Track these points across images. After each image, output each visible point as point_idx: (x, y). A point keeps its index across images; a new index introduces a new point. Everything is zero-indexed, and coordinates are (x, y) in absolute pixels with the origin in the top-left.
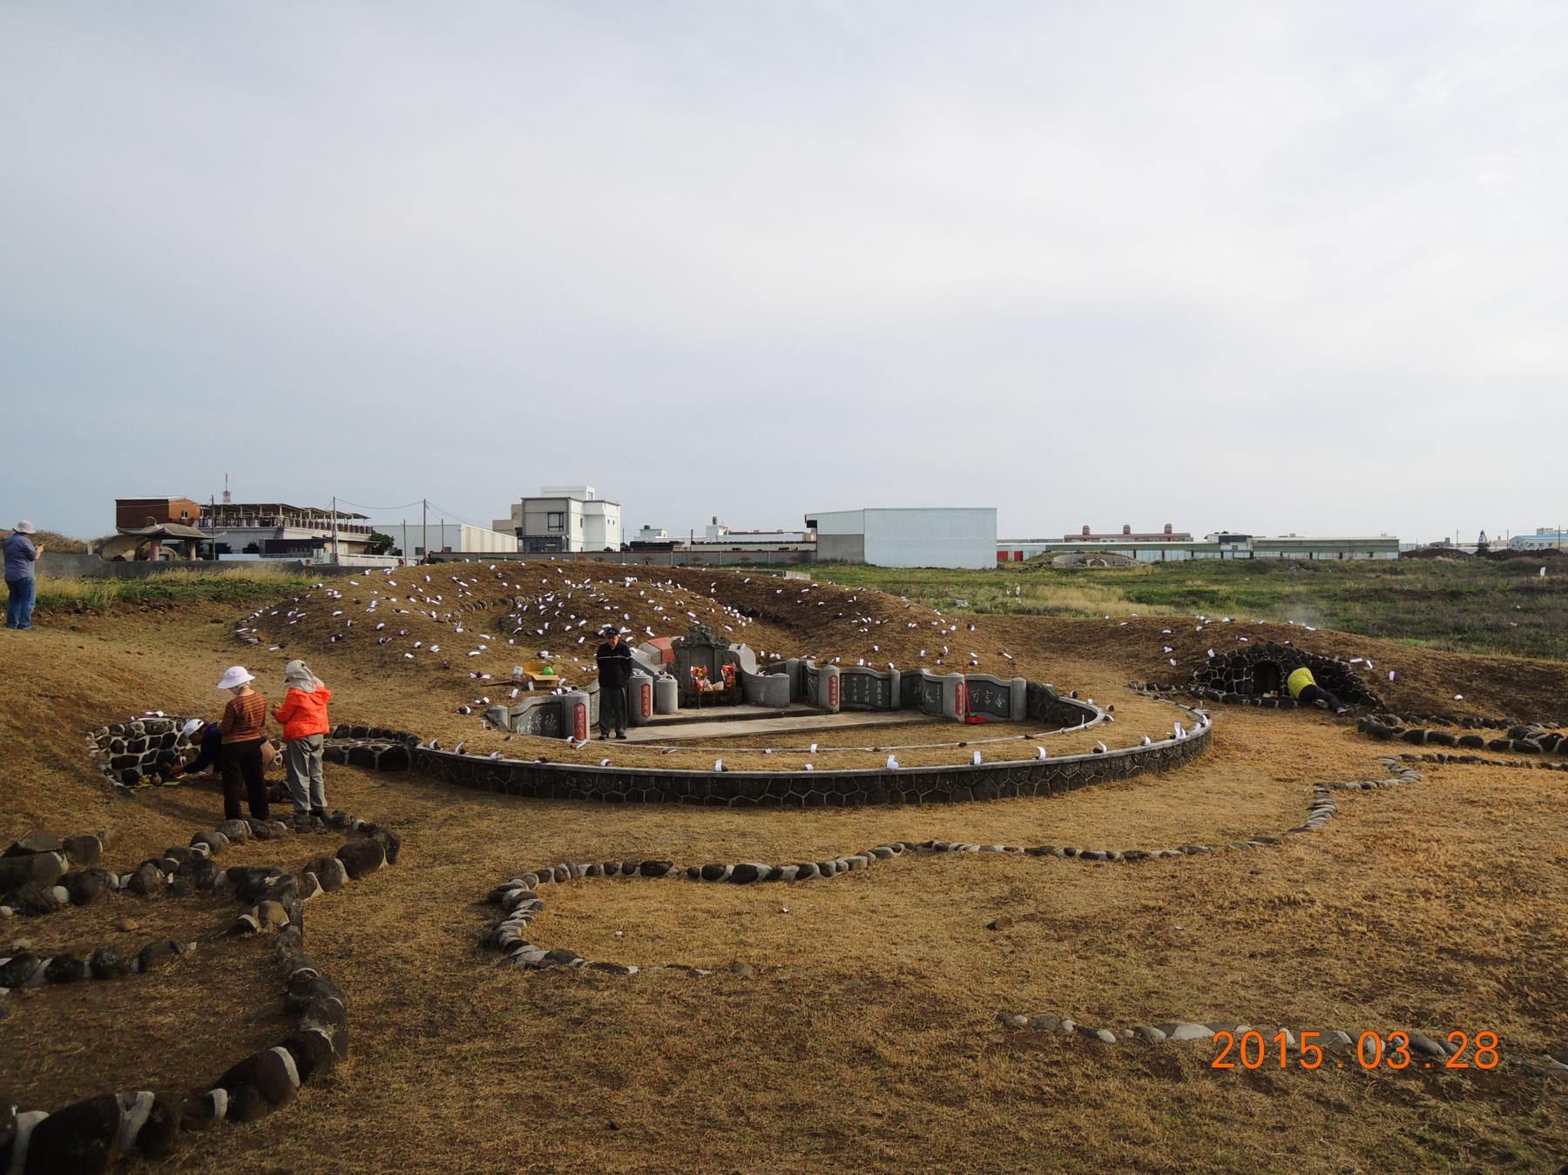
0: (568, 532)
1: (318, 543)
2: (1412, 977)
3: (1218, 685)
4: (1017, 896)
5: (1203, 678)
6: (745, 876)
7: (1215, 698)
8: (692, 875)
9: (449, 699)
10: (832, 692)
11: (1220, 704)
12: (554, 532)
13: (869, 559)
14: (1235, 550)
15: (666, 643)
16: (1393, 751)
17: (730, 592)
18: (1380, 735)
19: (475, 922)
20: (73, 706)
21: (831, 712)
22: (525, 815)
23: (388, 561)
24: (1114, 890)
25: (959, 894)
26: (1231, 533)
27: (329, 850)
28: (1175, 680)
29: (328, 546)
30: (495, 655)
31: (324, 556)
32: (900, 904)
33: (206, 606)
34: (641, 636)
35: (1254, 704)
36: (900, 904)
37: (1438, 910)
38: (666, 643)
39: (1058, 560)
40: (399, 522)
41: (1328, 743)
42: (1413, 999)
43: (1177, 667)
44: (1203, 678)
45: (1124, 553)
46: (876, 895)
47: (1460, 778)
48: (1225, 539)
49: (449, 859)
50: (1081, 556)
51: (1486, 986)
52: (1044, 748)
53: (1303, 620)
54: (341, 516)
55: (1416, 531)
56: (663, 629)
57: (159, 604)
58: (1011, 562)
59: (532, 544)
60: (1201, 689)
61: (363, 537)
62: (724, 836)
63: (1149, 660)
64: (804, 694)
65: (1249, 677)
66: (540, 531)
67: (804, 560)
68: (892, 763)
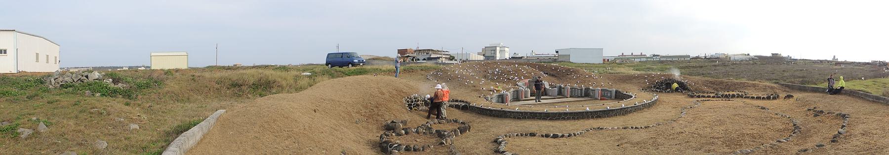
0: (49, 75)
1: (439, 58)
2: (707, 144)
4: (622, 138)
6: (555, 136)
8: (542, 136)
9: (476, 94)
10: (568, 92)
15: (527, 81)
16: (695, 99)
17: (541, 68)
18: (692, 97)
19: (493, 146)
20: (400, 92)
22: (498, 121)
23: (453, 62)
24: (643, 135)
25: (608, 139)
27: (456, 128)
28: (648, 87)
30: (485, 84)
31: (440, 61)
32: (594, 142)
34: (520, 79)
36: (594, 142)
37: (709, 130)
38: (527, 81)
41: (681, 99)
42: (707, 147)
46: (588, 140)
47: (709, 104)
48: (654, 55)
49: (482, 131)
51: (720, 143)
52: (623, 104)
53: (676, 74)
55: (693, 54)
56: (526, 77)
57: (410, 71)
58: (606, 62)
59: (487, 58)
62: (548, 127)
64: (561, 93)
65: (665, 86)
66: (489, 54)
67: (555, 61)
68: (588, 109)
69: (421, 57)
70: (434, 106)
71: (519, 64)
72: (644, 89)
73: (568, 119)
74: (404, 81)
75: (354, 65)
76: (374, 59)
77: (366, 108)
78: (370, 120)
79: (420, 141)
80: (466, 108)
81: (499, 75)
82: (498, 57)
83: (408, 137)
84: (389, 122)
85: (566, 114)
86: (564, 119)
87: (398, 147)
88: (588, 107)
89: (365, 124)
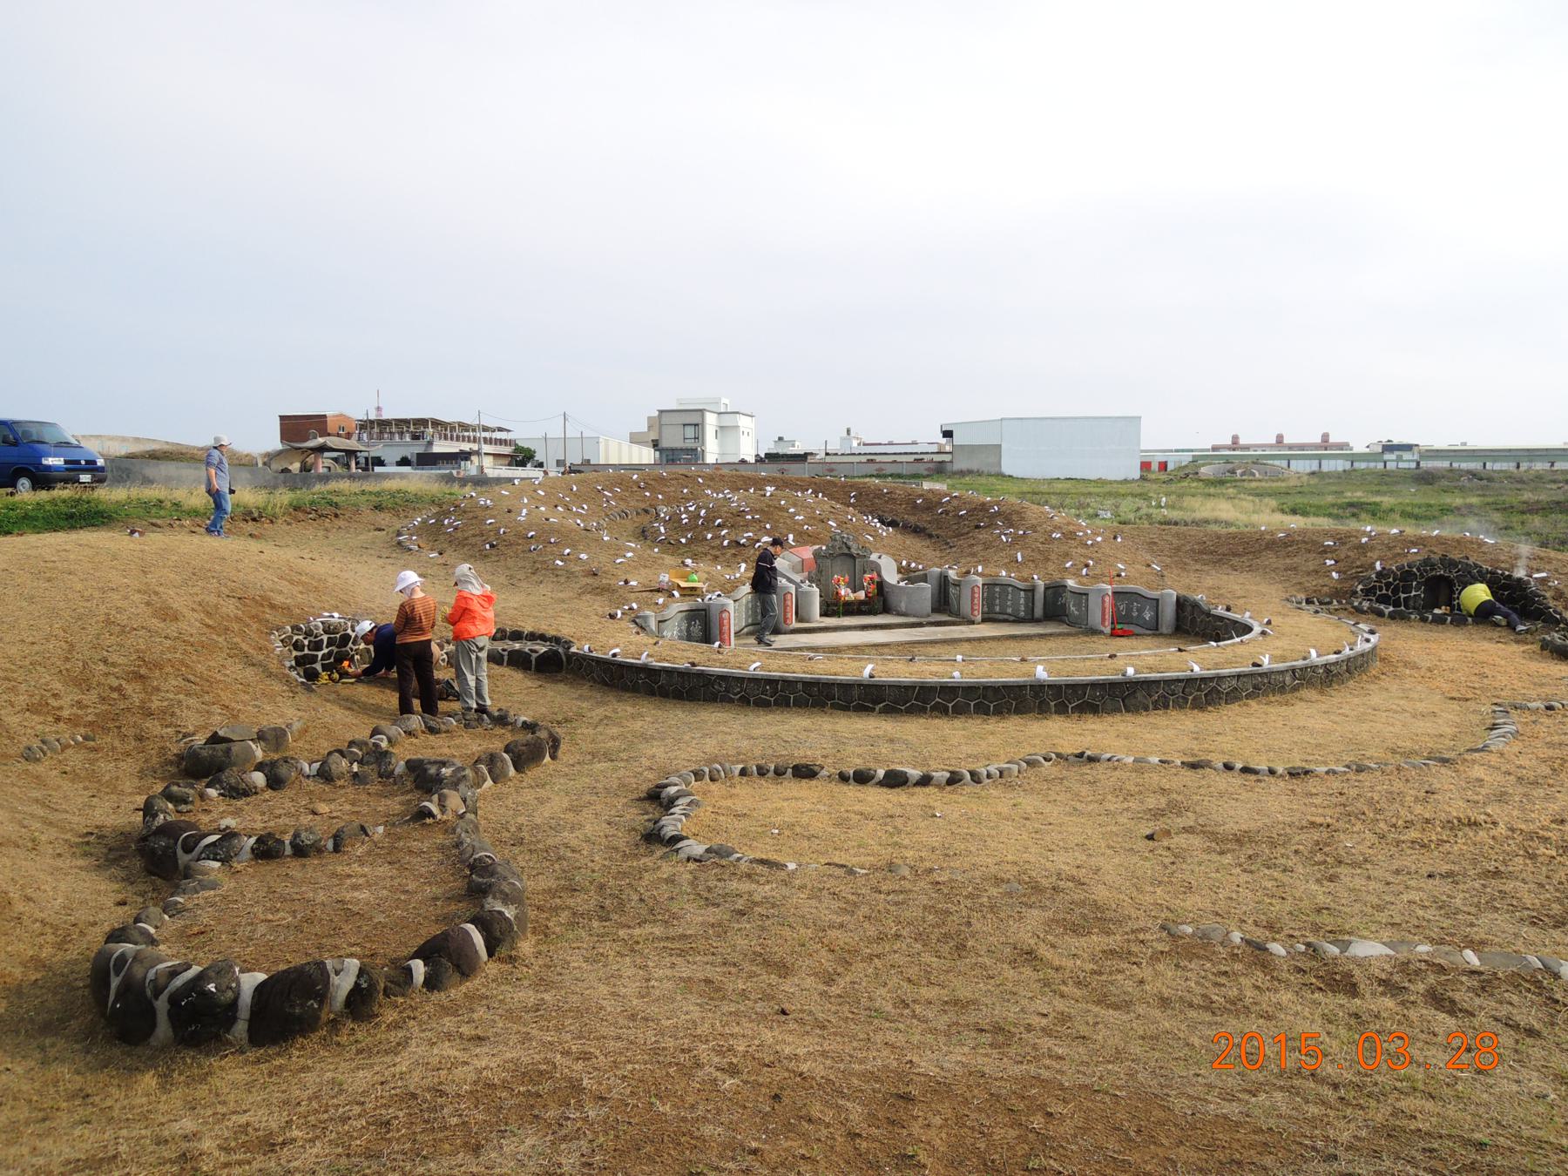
0: (703, 444)
1: (465, 456)
3: (1384, 600)
4: (1175, 808)
5: (1368, 592)
7: (1380, 614)
8: (843, 778)
9: (600, 605)
10: (971, 599)
11: (1385, 620)
12: (690, 444)
13: (1006, 469)
14: (1399, 459)
15: (807, 552)
20: (257, 606)
21: (973, 623)
24: (1275, 805)
25: (1113, 804)
26: (1395, 442)
27: (497, 745)
28: (1337, 594)
30: (641, 563)
31: (470, 468)
32: (1053, 812)
33: (368, 515)
35: (1424, 620)
36: (1053, 812)
38: (807, 552)
39: (1205, 471)
40: (540, 435)
41: (1507, 661)
43: (1340, 581)
44: (1368, 592)
45: (1277, 463)
46: (1029, 803)
48: (1389, 448)
49: (608, 756)
50: (1229, 466)
52: (1198, 660)
54: (486, 429)
56: (804, 538)
57: (327, 512)
58: (1155, 472)
59: (669, 456)
60: (1366, 605)
61: (507, 450)
62: (873, 741)
63: (1309, 574)
64: (945, 603)
65: (1421, 591)
68: (1041, 673)
69: (391, 453)
70: (400, 660)
71: (782, 484)
72: (1320, 600)
73: (960, 711)
74: (289, 555)
75: (43, 479)
76: (154, 456)
77: (82, 682)
78: (105, 740)
79: (335, 808)
80: (555, 663)
81: (698, 527)
82: (713, 452)
83: (282, 802)
84: (200, 739)
85: (949, 691)
86: (941, 711)
87: (225, 847)
88: (1046, 661)
89: (75, 759)
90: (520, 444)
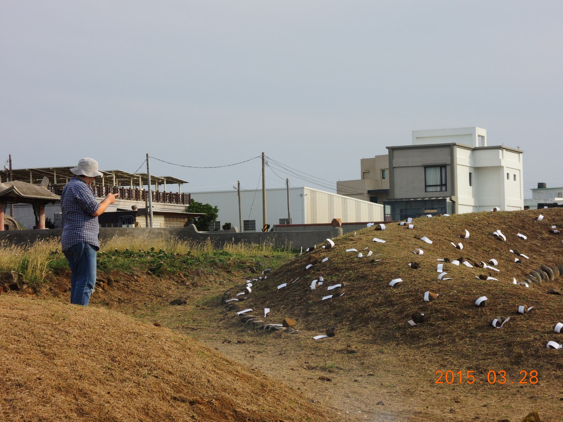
0: (453, 192)
12: (434, 193)
29: (141, 221)
33: (145, 281)
40: (230, 186)
54: (157, 181)
61: (179, 208)
82: (465, 200)
90: (197, 199)
